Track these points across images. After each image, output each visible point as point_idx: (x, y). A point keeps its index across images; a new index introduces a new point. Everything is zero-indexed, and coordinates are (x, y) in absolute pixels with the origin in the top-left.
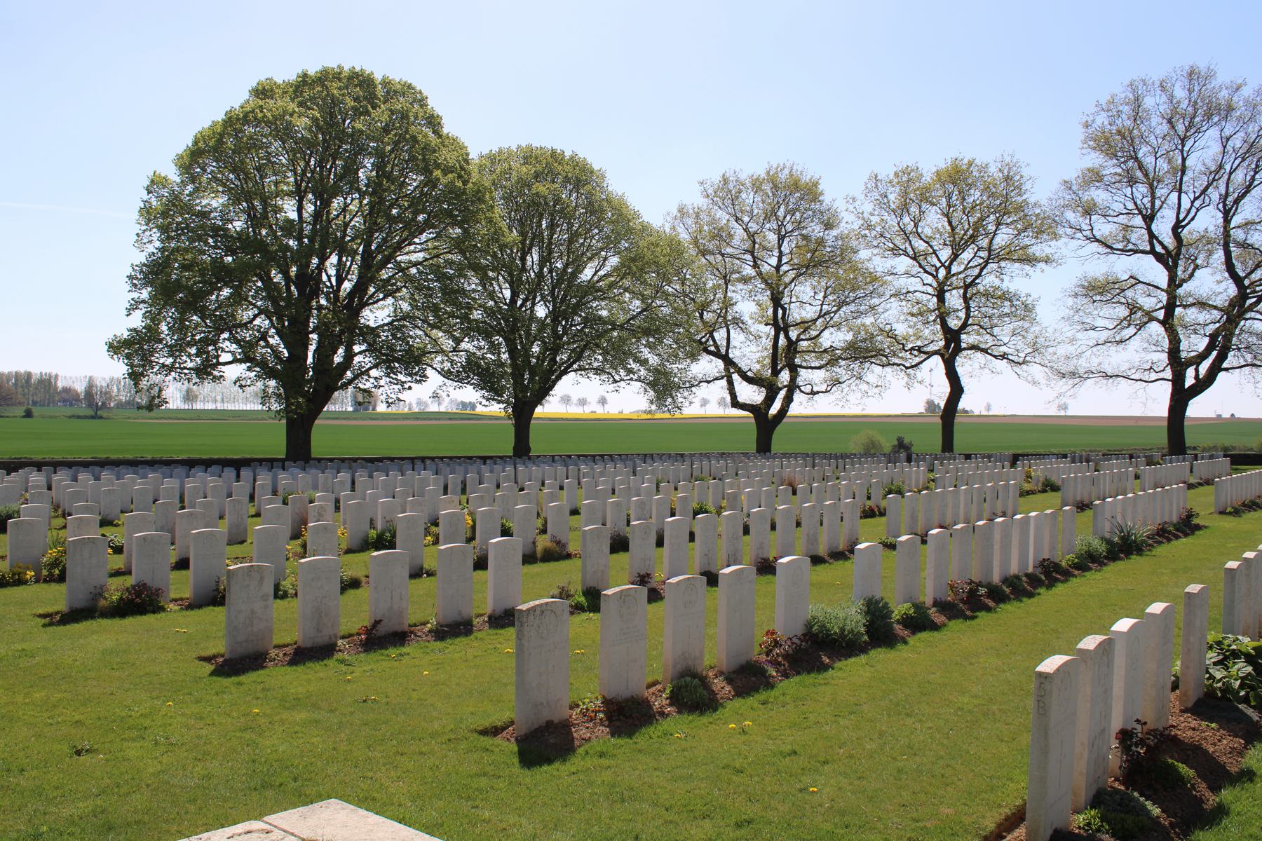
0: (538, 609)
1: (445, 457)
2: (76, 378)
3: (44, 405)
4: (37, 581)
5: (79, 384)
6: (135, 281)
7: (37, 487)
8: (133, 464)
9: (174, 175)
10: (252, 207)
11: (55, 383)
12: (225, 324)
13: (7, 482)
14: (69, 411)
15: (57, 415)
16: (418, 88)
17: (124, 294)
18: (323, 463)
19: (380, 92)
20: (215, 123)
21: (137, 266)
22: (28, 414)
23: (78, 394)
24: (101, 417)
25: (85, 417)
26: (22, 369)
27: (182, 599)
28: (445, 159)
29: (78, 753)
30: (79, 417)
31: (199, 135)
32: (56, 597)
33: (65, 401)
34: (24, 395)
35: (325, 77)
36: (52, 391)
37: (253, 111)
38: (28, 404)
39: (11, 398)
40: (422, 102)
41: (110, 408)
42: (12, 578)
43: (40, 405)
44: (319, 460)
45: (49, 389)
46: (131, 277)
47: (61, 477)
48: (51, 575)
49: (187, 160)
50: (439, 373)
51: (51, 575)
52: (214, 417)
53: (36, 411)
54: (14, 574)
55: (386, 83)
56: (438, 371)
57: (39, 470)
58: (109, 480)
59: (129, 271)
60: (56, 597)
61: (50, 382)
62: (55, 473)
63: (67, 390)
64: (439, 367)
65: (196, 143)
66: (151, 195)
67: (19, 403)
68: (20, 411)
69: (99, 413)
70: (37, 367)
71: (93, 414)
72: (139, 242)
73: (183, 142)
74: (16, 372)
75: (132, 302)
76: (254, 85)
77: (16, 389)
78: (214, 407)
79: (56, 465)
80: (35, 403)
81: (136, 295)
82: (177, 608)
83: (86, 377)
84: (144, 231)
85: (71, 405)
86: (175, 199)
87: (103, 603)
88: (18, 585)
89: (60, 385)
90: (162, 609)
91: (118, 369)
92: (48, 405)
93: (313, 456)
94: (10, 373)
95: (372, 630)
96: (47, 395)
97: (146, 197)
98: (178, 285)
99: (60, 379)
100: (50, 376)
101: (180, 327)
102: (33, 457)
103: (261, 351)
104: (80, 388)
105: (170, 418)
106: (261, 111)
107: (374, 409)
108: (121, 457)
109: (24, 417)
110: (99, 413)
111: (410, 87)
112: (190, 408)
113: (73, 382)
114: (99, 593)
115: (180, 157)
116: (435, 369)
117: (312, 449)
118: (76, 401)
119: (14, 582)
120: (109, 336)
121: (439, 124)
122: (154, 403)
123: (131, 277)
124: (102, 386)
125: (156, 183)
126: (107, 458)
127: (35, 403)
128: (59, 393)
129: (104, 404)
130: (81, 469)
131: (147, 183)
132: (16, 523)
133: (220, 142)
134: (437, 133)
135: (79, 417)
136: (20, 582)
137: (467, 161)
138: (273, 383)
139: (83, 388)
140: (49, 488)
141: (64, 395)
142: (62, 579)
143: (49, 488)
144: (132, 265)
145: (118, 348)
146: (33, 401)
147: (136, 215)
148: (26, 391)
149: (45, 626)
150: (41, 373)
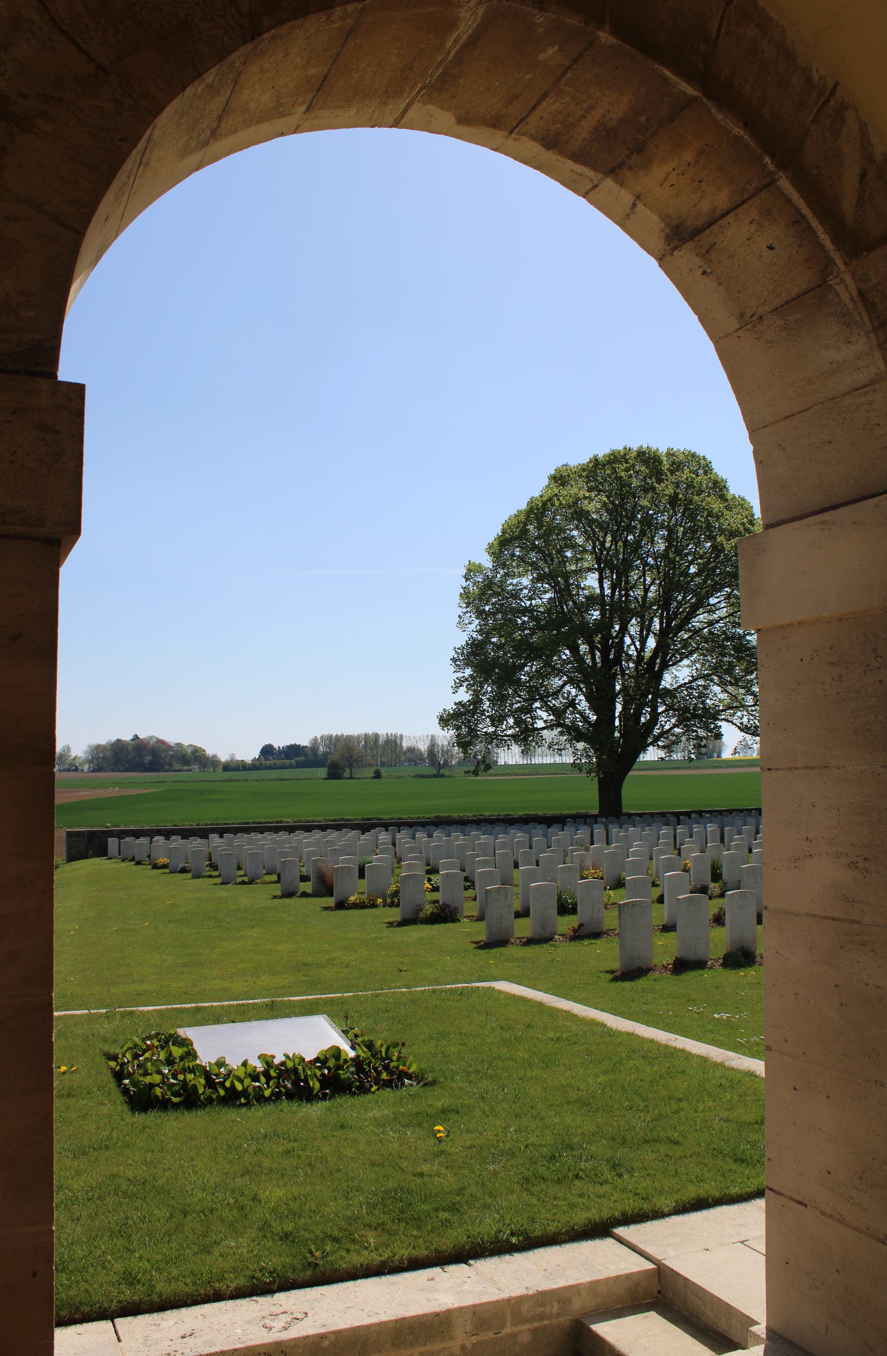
0: (630, 905)
1: (669, 813)
2: (420, 737)
3: (391, 765)
4: (384, 906)
5: (422, 743)
6: (457, 663)
7: (384, 843)
8: (479, 822)
9: (487, 562)
10: (557, 584)
11: (401, 743)
12: (538, 693)
13: (363, 840)
14: (414, 770)
15: (402, 775)
16: (701, 455)
17: (450, 675)
18: (632, 818)
19: (666, 466)
20: (519, 512)
21: (459, 649)
22: (378, 775)
23: (421, 754)
24: (443, 776)
25: (429, 776)
26: (370, 731)
27: (472, 916)
28: (729, 525)
29: (401, 971)
30: (423, 776)
31: (506, 526)
32: (395, 914)
33: (410, 760)
34: (373, 757)
35: (615, 459)
36: (398, 752)
37: (550, 499)
38: (377, 766)
39: (362, 760)
40: (707, 468)
41: (452, 766)
42: (369, 903)
43: (388, 766)
44: (630, 815)
45: (396, 749)
46: (454, 660)
47: (403, 836)
48: (392, 902)
49: (496, 548)
50: (739, 728)
51: (392, 902)
52: (552, 771)
53: (384, 771)
54: (370, 901)
55: (670, 454)
56: (737, 726)
57: (387, 830)
58: (439, 837)
59: (453, 654)
60: (395, 914)
61: (395, 741)
62: (399, 832)
63: (411, 750)
64: (737, 722)
65: (504, 532)
66: (468, 582)
67: (369, 765)
68: (370, 772)
69: (441, 771)
70: (383, 728)
71: (436, 772)
72: (461, 623)
73: (493, 531)
74: (365, 734)
75: (457, 681)
76: (553, 472)
77: (366, 751)
78: (552, 761)
79: (399, 825)
80: (383, 764)
81: (460, 675)
82: (468, 921)
83: (428, 736)
84: (465, 613)
85: (416, 764)
86: (489, 584)
87: (421, 915)
88: (372, 908)
89: (405, 744)
90: (458, 921)
91: (446, 736)
92: (395, 766)
93: (624, 811)
94: (359, 736)
95: (578, 930)
96: (394, 755)
97: (465, 584)
98: (495, 662)
99: (404, 738)
100: (396, 736)
101: (499, 699)
102: (382, 817)
103: (569, 717)
104: (423, 747)
105: (508, 774)
106: (558, 499)
107: (719, 756)
108: (461, 815)
109: (374, 778)
110: (441, 771)
111: (694, 455)
112: (529, 762)
113: (417, 742)
114: (419, 909)
115: (491, 546)
116: (735, 724)
117: (624, 803)
118: (420, 760)
119: (370, 905)
120: (439, 711)
121: (725, 487)
122: (486, 765)
123: (454, 660)
124: (443, 746)
125: (472, 570)
126: (449, 816)
127: (383, 764)
128: (405, 753)
129: (446, 762)
130: (420, 828)
131: (464, 571)
132: (370, 866)
133: (525, 531)
134: (723, 498)
135: (423, 776)
136: (374, 906)
137: (751, 523)
138: (581, 745)
139: (426, 747)
140: (394, 845)
141: (408, 755)
142: (398, 905)
143: (394, 845)
144: (455, 648)
145: (448, 720)
146: (381, 762)
147: (457, 599)
148: (375, 752)
149: (388, 927)
150: (387, 734)
